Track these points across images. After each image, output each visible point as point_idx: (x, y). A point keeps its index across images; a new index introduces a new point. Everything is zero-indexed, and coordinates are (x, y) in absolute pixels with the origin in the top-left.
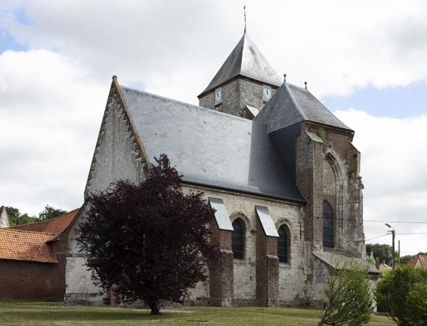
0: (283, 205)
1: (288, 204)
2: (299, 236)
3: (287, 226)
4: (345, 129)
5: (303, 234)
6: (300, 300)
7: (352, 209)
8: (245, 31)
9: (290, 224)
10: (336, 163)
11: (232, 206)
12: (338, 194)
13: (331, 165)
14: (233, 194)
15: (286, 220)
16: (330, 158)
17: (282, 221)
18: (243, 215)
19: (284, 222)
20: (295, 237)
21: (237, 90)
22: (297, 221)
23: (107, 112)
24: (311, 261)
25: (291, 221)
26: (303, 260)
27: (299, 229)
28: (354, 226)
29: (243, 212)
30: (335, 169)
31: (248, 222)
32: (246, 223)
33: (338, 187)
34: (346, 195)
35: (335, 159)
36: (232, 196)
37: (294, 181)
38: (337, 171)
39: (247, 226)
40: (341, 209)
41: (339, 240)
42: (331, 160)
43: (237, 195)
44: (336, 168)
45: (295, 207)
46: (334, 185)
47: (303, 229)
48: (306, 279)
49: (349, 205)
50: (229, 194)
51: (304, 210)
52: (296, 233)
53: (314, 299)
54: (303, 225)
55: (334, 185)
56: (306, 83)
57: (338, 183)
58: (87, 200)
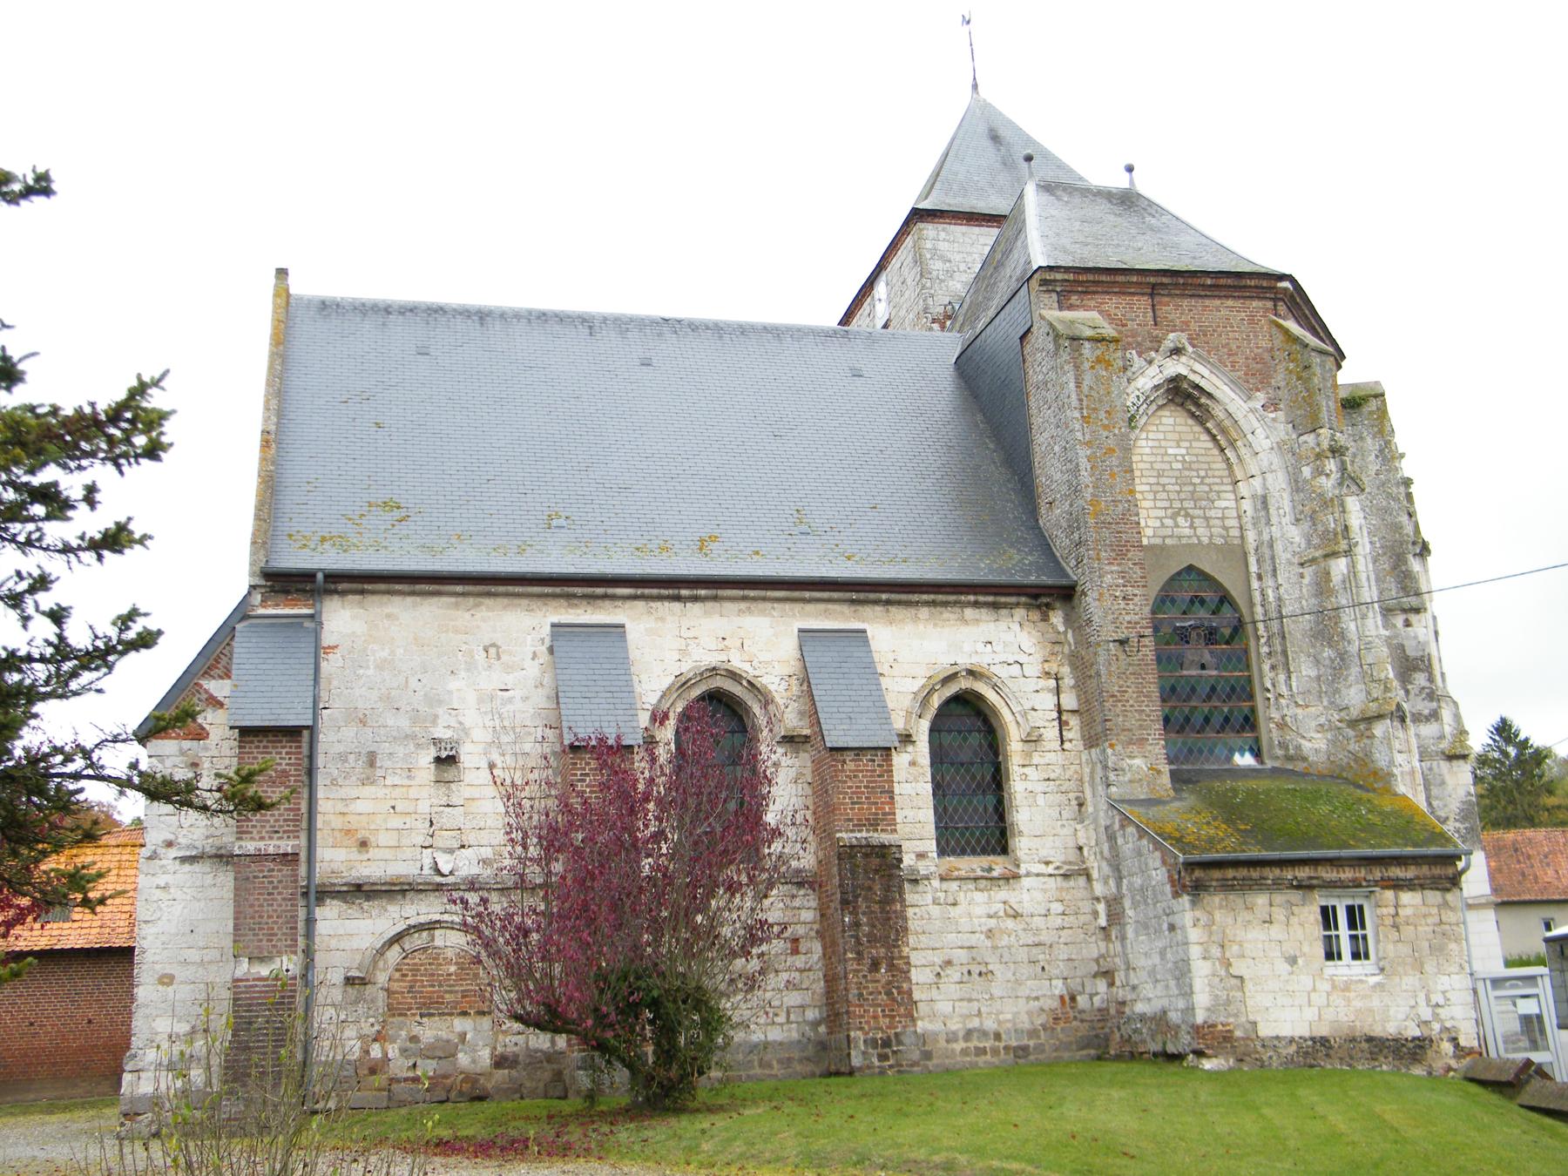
0: (947, 614)
1: (976, 604)
2: (1051, 733)
3: (980, 697)
4: (1239, 275)
5: (1074, 722)
6: (1080, 1016)
7: (1323, 586)
8: (975, 87)
9: (994, 687)
10: (1218, 412)
11: (681, 644)
12: (1251, 536)
13: (1201, 421)
14: (678, 598)
15: (971, 673)
16: (1181, 394)
17: (947, 680)
18: (734, 676)
19: (964, 684)
20: (1033, 740)
21: (919, 260)
22: (1033, 669)
23: (1184, 574)
24: (1112, 838)
25: (1002, 672)
26: (1085, 836)
27: (1049, 701)
28: (1342, 656)
29: (738, 664)
30: (1223, 437)
31: (766, 700)
32: (756, 709)
33: (1247, 505)
34: (1289, 535)
35: (1210, 395)
36: (677, 606)
37: (1033, 512)
38: (1232, 444)
39: (762, 720)
40: (1271, 594)
41: (1282, 725)
42: (1198, 405)
43: (695, 599)
44: (1224, 431)
45: (1020, 613)
46: (1227, 502)
47: (1069, 701)
48: (1103, 921)
49: (1308, 572)
50: (660, 598)
51: (1068, 621)
52: (1037, 719)
53: (1140, 1008)
54: (1068, 681)
55: (1227, 502)
56: (1130, 169)
57: (1243, 488)
58: (1538, 752)
